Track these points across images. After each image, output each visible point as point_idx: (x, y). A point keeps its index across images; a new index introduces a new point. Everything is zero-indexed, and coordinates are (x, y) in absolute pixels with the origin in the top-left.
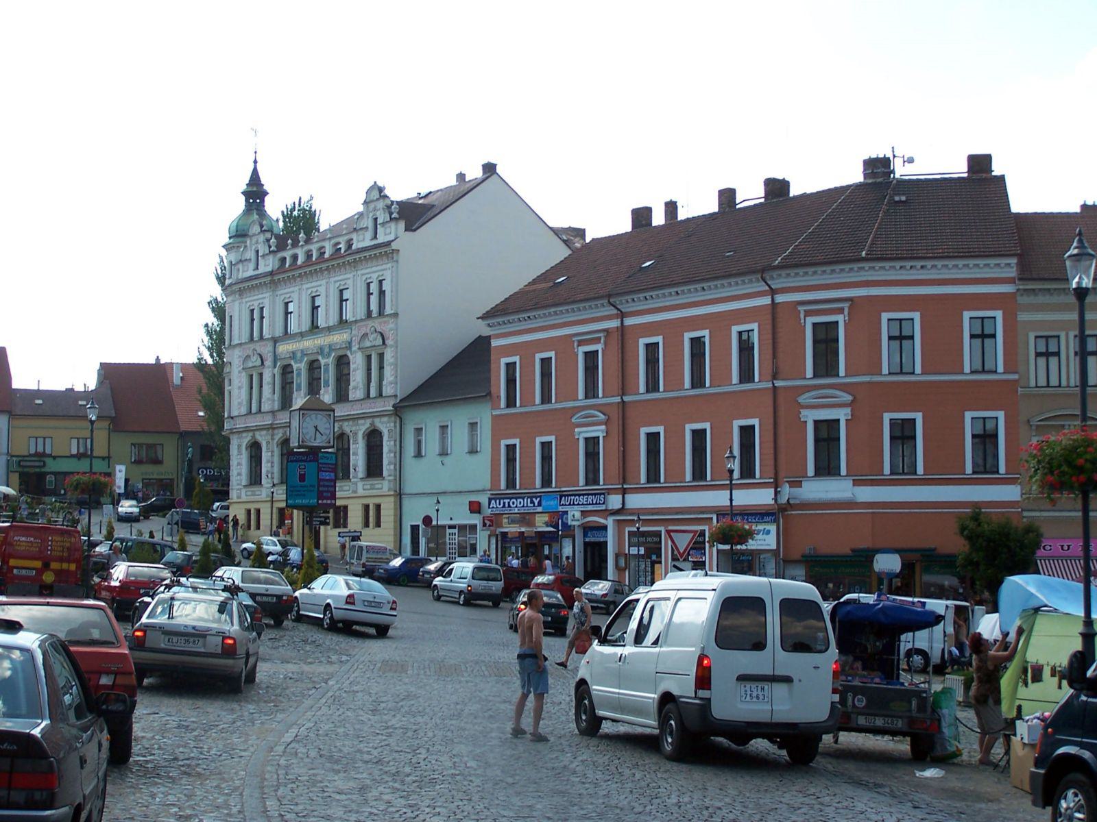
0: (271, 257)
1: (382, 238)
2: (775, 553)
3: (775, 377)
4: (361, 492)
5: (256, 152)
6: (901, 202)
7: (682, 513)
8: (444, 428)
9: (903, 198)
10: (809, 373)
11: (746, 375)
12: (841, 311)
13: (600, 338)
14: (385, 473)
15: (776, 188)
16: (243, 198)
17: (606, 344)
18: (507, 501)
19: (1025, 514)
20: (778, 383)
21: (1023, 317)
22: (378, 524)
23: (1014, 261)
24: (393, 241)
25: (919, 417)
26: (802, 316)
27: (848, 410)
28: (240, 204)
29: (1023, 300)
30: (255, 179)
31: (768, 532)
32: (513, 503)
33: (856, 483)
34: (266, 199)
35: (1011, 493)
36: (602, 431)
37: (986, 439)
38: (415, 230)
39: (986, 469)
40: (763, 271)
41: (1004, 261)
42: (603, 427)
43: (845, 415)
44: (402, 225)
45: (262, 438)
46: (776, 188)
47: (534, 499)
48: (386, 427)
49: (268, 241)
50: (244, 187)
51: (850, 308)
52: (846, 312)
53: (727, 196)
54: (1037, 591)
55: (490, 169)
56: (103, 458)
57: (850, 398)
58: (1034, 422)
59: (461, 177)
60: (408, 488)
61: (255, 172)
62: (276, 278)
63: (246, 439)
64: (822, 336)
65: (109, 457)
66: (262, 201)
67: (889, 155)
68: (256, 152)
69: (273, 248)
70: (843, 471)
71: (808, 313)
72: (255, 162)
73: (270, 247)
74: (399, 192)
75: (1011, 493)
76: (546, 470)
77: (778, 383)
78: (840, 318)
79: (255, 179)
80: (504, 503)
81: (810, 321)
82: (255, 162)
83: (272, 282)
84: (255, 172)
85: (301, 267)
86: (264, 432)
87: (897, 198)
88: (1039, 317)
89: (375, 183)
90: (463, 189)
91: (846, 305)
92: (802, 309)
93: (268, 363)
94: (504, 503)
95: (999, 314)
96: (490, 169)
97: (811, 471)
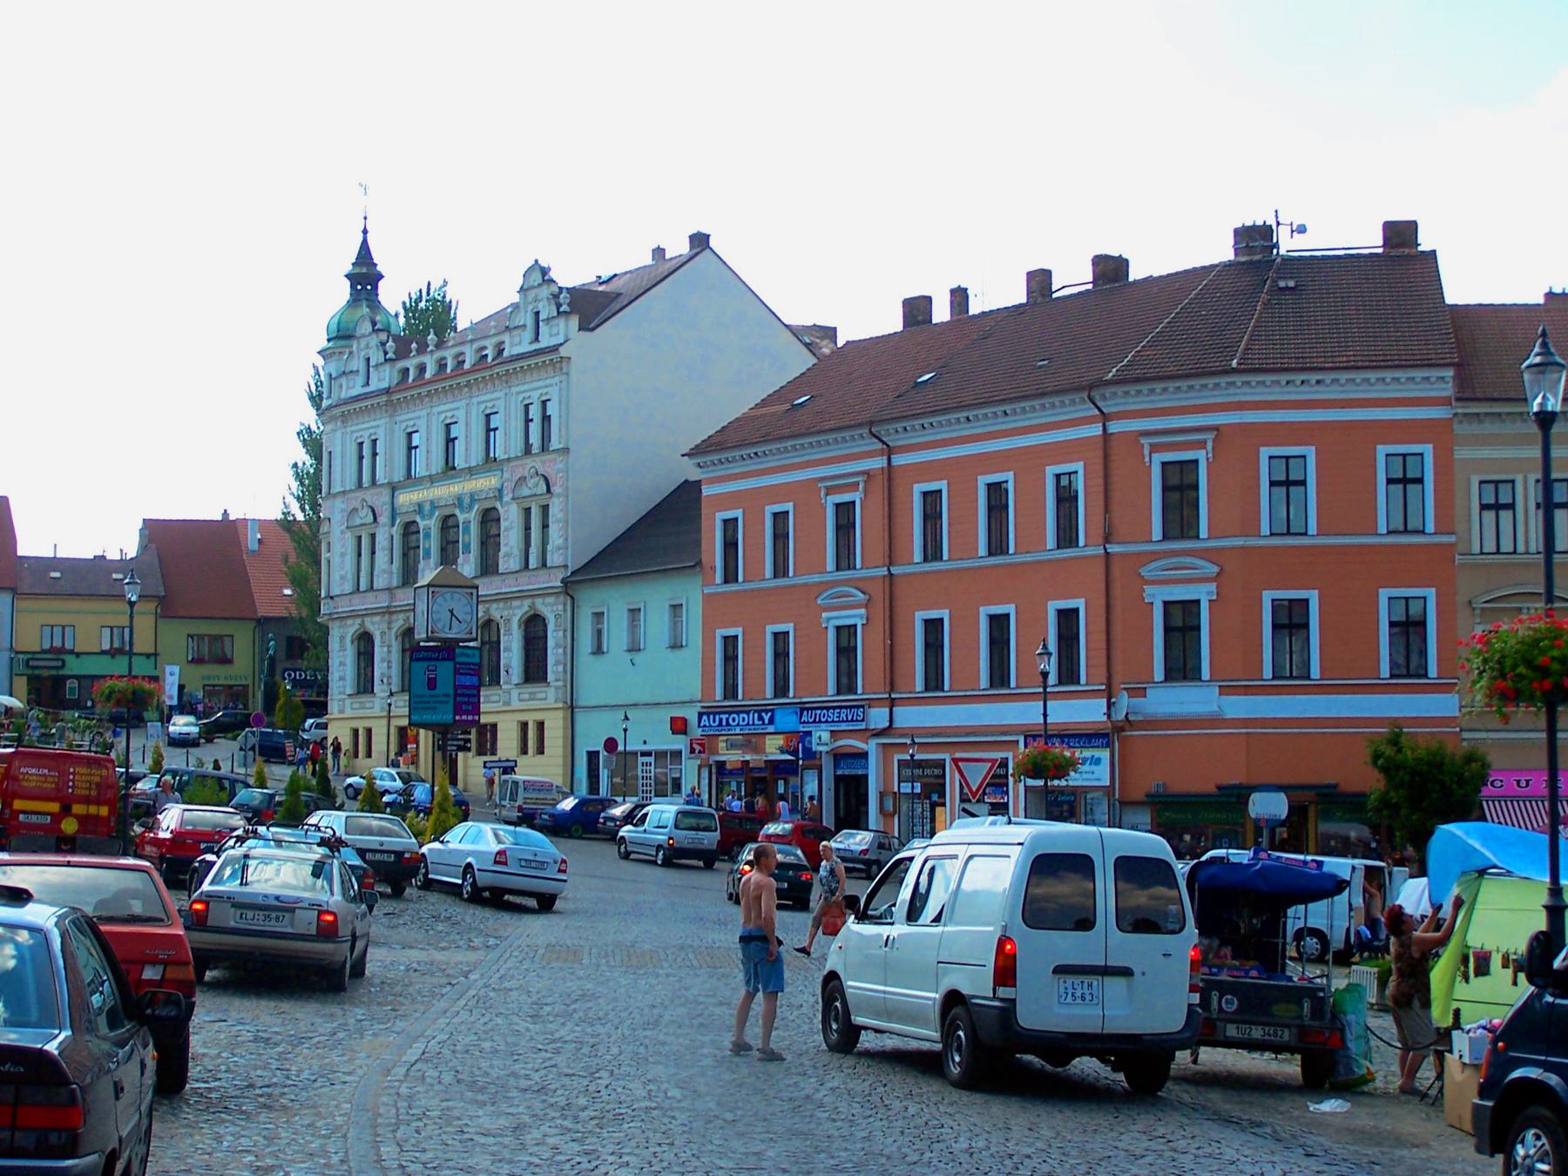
0: (387, 367)
1: (545, 341)
2: (1109, 790)
3: (1107, 539)
4: (516, 704)
5: (365, 218)
6: (1287, 288)
7: (967, 735)
8: (634, 612)
9: (1291, 284)
10: (1157, 533)
11: (1067, 536)
12: (1201, 445)
13: (857, 484)
14: (550, 677)
15: (1110, 269)
16: (348, 283)
17: (866, 491)
18: (724, 717)
19: (1466, 735)
20: (1112, 549)
21: (1461, 453)
22: (541, 750)
23: (1449, 373)
24: (561, 344)
25: (1313, 597)
26: (1146, 452)
27: (1213, 587)
28: (342, 292)
29: (1460, 429)
30: (365, 255)
31: (1098, 761)
32: (734, 720)
33: (1224, 690)
34: (381, 284)
35: (1443, 705)
36: (861, 617)
37: (1409, 629)
38: (593, 329)
39: (1409, 668)
40: (1091, 388)
41: (1435, 373)
42: (863, 611)
43: (1209, 593)
44: (574, 321)
45: (375, 626)
46: (1110, 269)
47: (764, 714)
48: (551, 610)
49: (383, 344)
50: (349, 268)
51: (1214, 441)
52: (1210, 445)
53: (1040, 280)
54: (1482, 846)
55: (700, 241)
56: (148, 656)
57: (1216, 569)
58: (1478, 605)
59: (659, 252)
60: (584, 698)
61: (365, 246)
62: (395, 397)
63: (352, 628)
64: (1174, 481)
65: (156, 655)
66: (376, 287)
67: (1271, 222)
68: (365, 218)
69: (391, 355)
70: (1206, 674)
71: (1155, 448)
72: (365, 232)
73: (386, 353)
74: (570, 275)
75: (1443, 705)
76: (781, 672)
77: (1112, 549)
78: (1200, 455)
79: (365, 255)
80: (721, 720)
81: (1158, 458)
82: (365, 232)
83: (389, 403)
84: (365, 246)
85: (430, 382)
86: (377, 619)
87: (1282, 284)
88: (1485, 453)
89: (1551, 288)
90: (662, 270)
91: (1209, 436)
92: (1145, 441)
93: (384, 519)
94: (721, 720)
95: (1427, 449)
96: (700, 241)
97: (1159, 674)
